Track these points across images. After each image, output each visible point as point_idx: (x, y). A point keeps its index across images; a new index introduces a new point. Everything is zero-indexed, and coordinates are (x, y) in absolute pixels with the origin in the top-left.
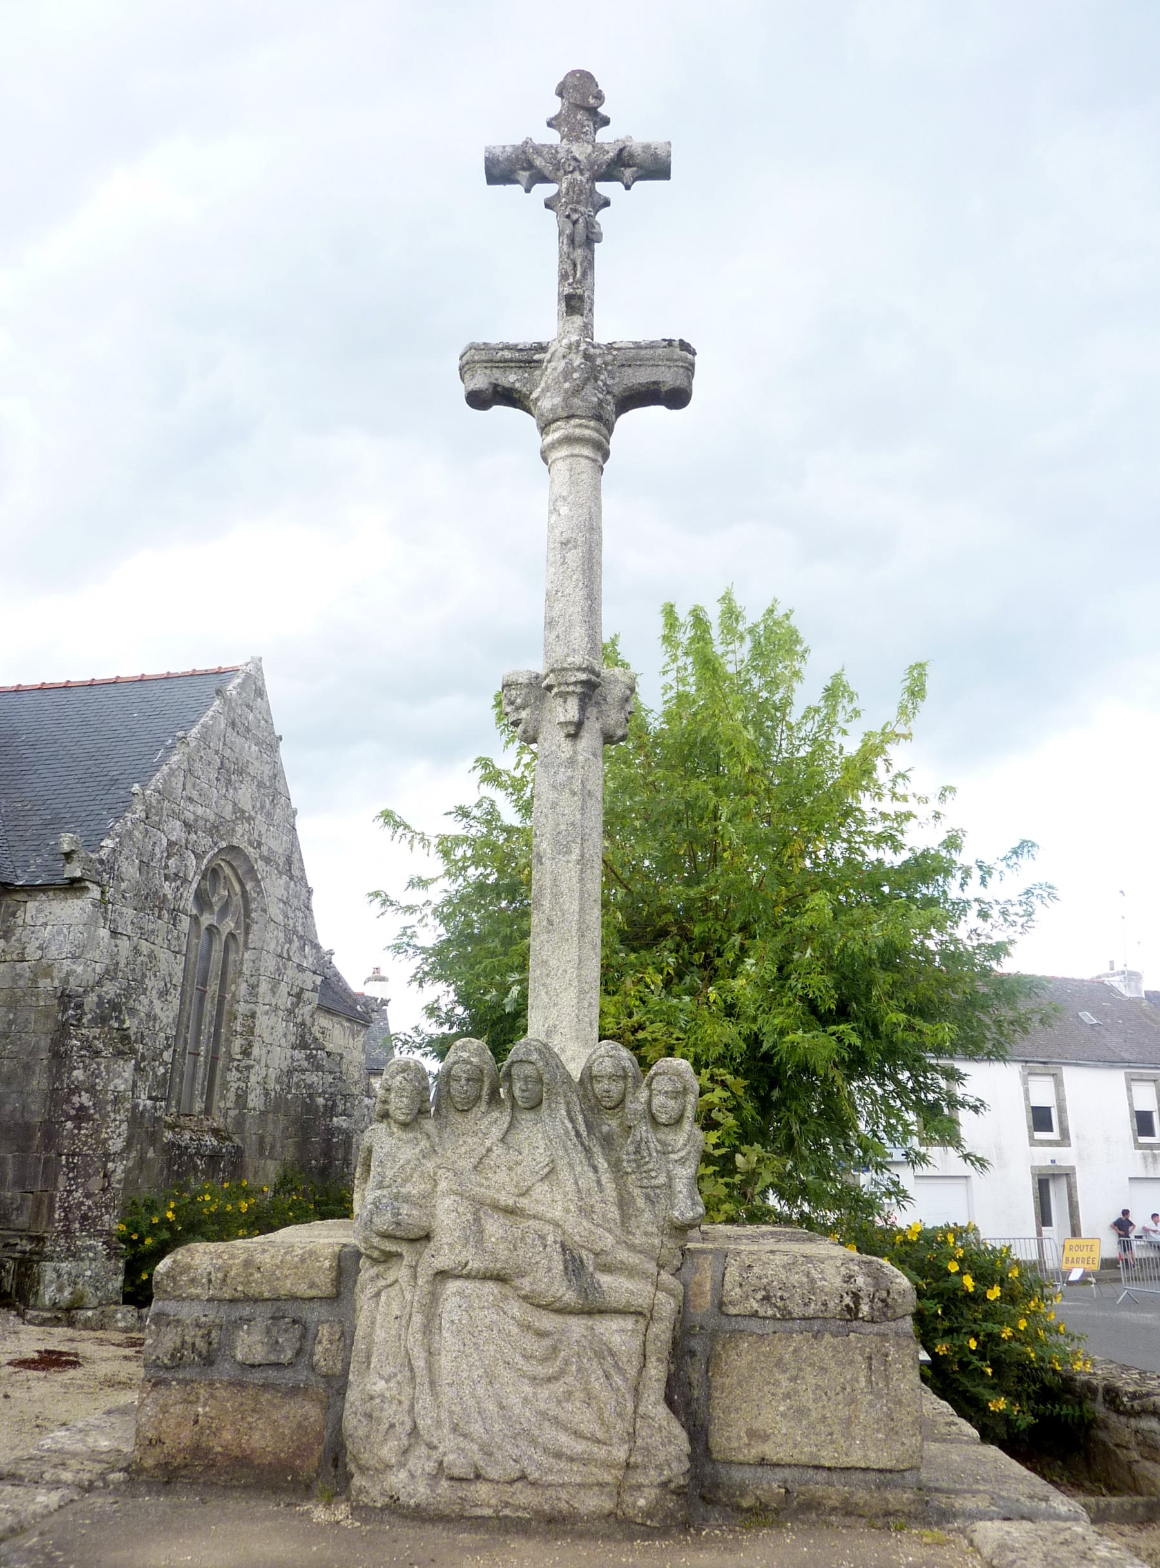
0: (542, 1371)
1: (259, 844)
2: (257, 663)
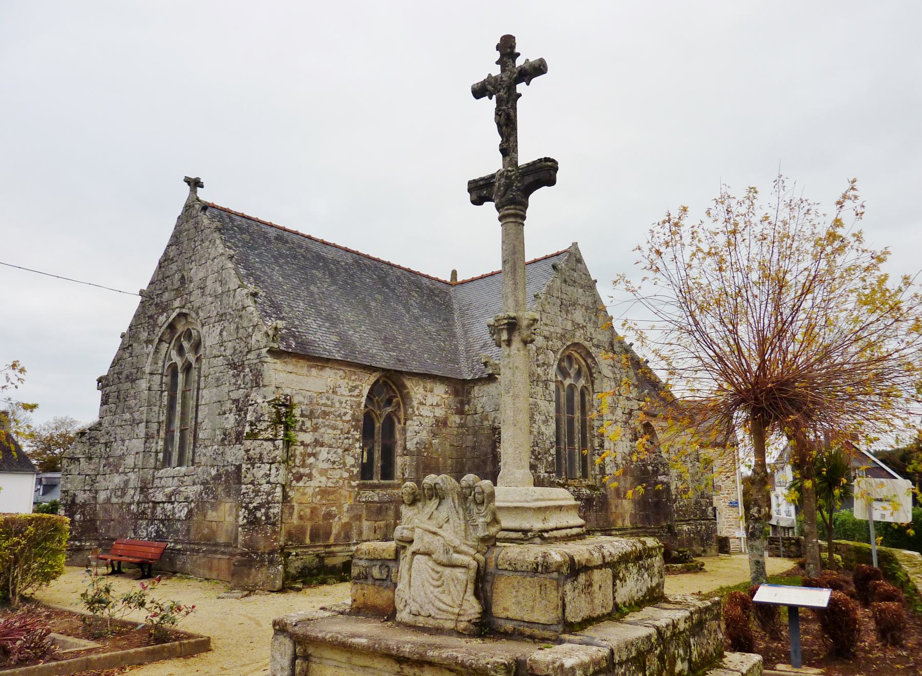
0: (439, 583)
1: (591, 339)
2: (575, 245)
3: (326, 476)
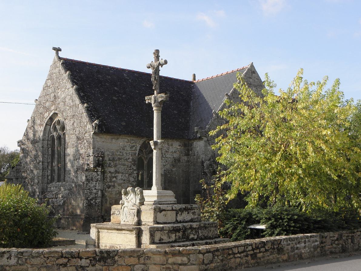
3: (121, 186)
